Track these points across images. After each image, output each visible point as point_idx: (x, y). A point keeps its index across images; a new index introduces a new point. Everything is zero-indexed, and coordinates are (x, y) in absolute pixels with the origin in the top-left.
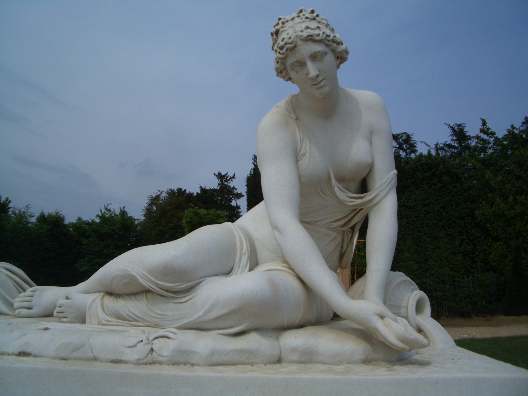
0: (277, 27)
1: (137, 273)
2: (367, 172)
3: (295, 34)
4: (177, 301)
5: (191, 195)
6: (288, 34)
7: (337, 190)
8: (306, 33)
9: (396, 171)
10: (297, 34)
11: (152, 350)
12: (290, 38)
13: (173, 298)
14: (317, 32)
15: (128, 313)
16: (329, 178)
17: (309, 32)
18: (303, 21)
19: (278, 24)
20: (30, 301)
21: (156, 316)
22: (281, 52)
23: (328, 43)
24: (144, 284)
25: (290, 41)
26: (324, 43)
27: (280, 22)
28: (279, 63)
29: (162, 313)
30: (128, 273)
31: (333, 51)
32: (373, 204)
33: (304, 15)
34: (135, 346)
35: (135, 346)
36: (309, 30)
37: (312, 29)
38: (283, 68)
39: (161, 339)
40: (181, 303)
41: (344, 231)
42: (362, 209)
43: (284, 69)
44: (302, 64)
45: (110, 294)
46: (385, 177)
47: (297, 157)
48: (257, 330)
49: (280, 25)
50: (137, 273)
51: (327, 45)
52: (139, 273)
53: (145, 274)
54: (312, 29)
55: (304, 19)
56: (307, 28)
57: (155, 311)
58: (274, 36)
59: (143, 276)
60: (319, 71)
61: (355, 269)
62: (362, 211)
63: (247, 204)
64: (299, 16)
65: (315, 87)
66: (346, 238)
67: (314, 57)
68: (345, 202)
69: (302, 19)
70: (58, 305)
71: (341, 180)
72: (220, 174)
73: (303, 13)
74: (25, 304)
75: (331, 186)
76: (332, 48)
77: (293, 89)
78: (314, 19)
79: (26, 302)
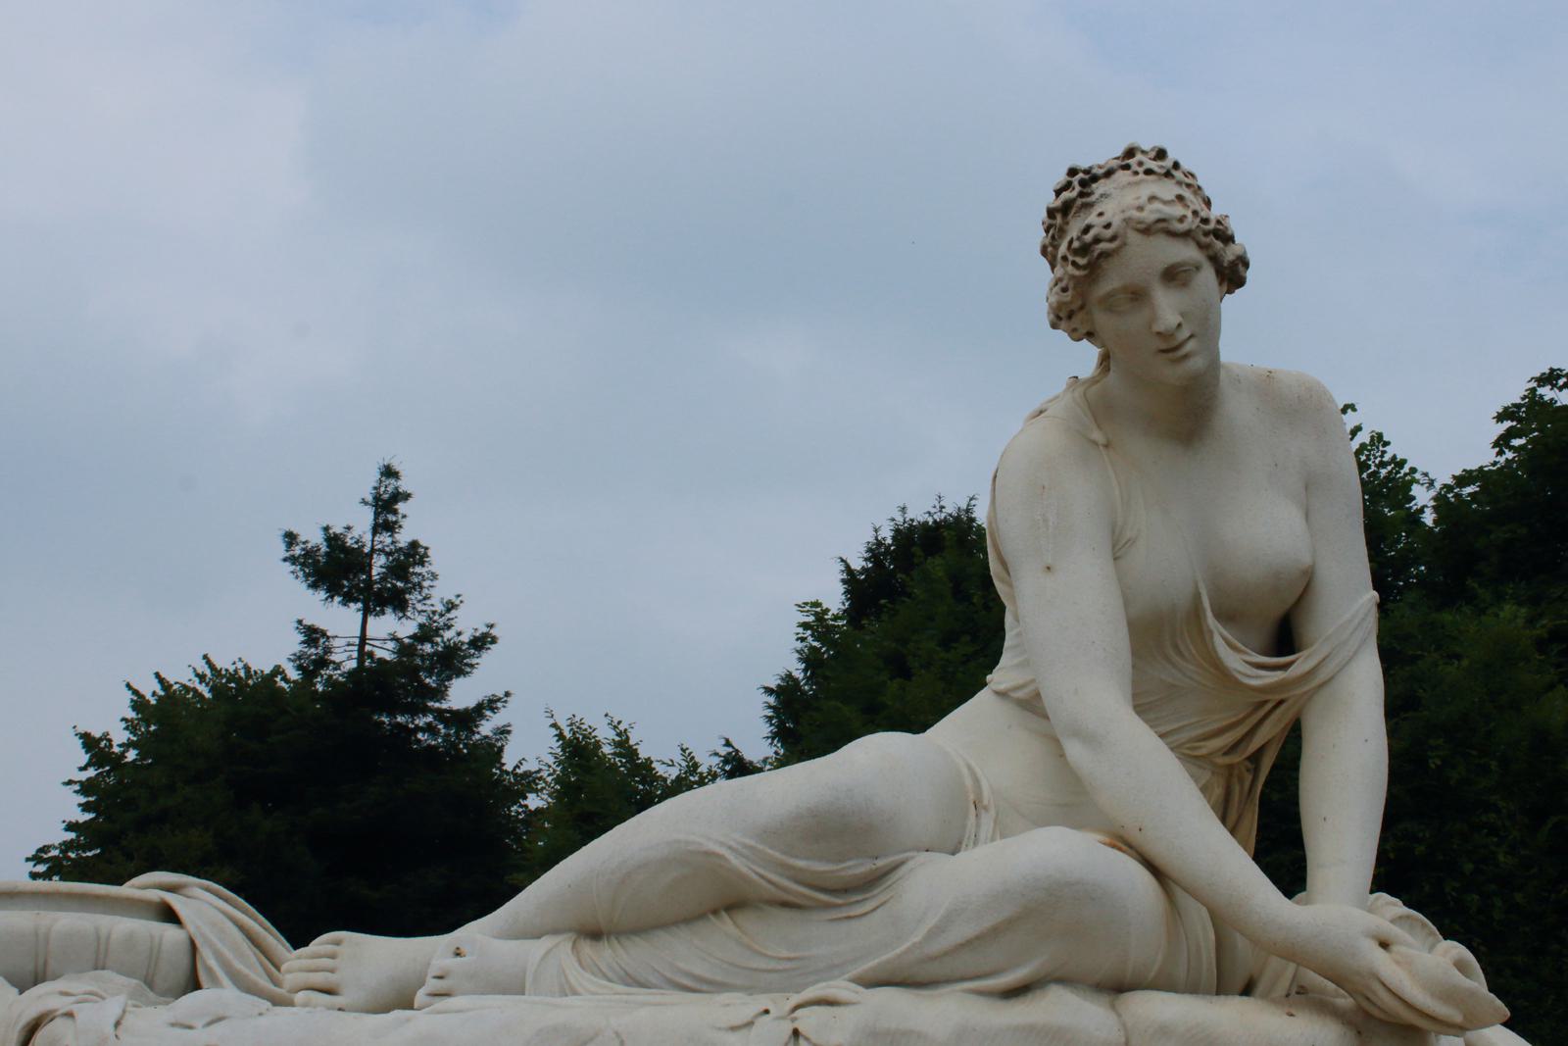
0: (1066, 195)
1: (722, 844)
2: (1291, 600)
3: (1122, 216)
4: (840, 915)
6: (1101, 214)
7: (1219, 642)
8: (1151, 212)
9: (1376, 593)
10: (1128, 214)
11: (796, 1033)
12: (1108, 226)
13: (828, 906)
14: (1178, 210)
15: (669, 975)
16: (1196, 613)
17: (1159, 211)
18: (1141, 181)
19: (1068, 186)
20: (332, 971)
21: (772, 965)
22: (1082, 261)
23: (1204, 240)
24: (744, 870)
25: (1109, 233)
26: (1194, 239)
27: (1076, 180)
28: (1070, 293)
29: (792, 955)
30: (691, 848)
31: (1215, 259)
32: (1317, 685)
33: (1140, 164)
34: (750, 1024)
35: (750, 1024)
36: (1157, 205)
37: (1165, 203)
38: (1079, 303)
39: (816, 1008)
40: (849, 918)
41: (1230, 767)
42: (1280, 703)
43: (1082, 308)
44: (1137, 295)
45: (595, 935)
46: (1349, 605)
47: (1118, 548)
48: (1063, 980)
49: (1078, 189)
50: (722, 844)
51: (1201, 246)
52: (732, 843)
53: (752, 843)
54: (1165, 203)
55: (1141, 176)
57: (769, 953)
59: (745, 851)
60: (1182, 315)
61: (1284, 858)
62: (1283, 707)
64: (1127, 167)
65: (1165, 355)
66: (1236, 789)
67: (1174, 275)
68: (1240, 677)
70: (433, 971)
71: (1226, 616)
72: (509, 732)
73: (1139, 157)
74: (319, 978)
75: (1201, 632)
76: (1211, 253)
77: (1085, 357)
78: (1168, 174)
79: (322, 971)
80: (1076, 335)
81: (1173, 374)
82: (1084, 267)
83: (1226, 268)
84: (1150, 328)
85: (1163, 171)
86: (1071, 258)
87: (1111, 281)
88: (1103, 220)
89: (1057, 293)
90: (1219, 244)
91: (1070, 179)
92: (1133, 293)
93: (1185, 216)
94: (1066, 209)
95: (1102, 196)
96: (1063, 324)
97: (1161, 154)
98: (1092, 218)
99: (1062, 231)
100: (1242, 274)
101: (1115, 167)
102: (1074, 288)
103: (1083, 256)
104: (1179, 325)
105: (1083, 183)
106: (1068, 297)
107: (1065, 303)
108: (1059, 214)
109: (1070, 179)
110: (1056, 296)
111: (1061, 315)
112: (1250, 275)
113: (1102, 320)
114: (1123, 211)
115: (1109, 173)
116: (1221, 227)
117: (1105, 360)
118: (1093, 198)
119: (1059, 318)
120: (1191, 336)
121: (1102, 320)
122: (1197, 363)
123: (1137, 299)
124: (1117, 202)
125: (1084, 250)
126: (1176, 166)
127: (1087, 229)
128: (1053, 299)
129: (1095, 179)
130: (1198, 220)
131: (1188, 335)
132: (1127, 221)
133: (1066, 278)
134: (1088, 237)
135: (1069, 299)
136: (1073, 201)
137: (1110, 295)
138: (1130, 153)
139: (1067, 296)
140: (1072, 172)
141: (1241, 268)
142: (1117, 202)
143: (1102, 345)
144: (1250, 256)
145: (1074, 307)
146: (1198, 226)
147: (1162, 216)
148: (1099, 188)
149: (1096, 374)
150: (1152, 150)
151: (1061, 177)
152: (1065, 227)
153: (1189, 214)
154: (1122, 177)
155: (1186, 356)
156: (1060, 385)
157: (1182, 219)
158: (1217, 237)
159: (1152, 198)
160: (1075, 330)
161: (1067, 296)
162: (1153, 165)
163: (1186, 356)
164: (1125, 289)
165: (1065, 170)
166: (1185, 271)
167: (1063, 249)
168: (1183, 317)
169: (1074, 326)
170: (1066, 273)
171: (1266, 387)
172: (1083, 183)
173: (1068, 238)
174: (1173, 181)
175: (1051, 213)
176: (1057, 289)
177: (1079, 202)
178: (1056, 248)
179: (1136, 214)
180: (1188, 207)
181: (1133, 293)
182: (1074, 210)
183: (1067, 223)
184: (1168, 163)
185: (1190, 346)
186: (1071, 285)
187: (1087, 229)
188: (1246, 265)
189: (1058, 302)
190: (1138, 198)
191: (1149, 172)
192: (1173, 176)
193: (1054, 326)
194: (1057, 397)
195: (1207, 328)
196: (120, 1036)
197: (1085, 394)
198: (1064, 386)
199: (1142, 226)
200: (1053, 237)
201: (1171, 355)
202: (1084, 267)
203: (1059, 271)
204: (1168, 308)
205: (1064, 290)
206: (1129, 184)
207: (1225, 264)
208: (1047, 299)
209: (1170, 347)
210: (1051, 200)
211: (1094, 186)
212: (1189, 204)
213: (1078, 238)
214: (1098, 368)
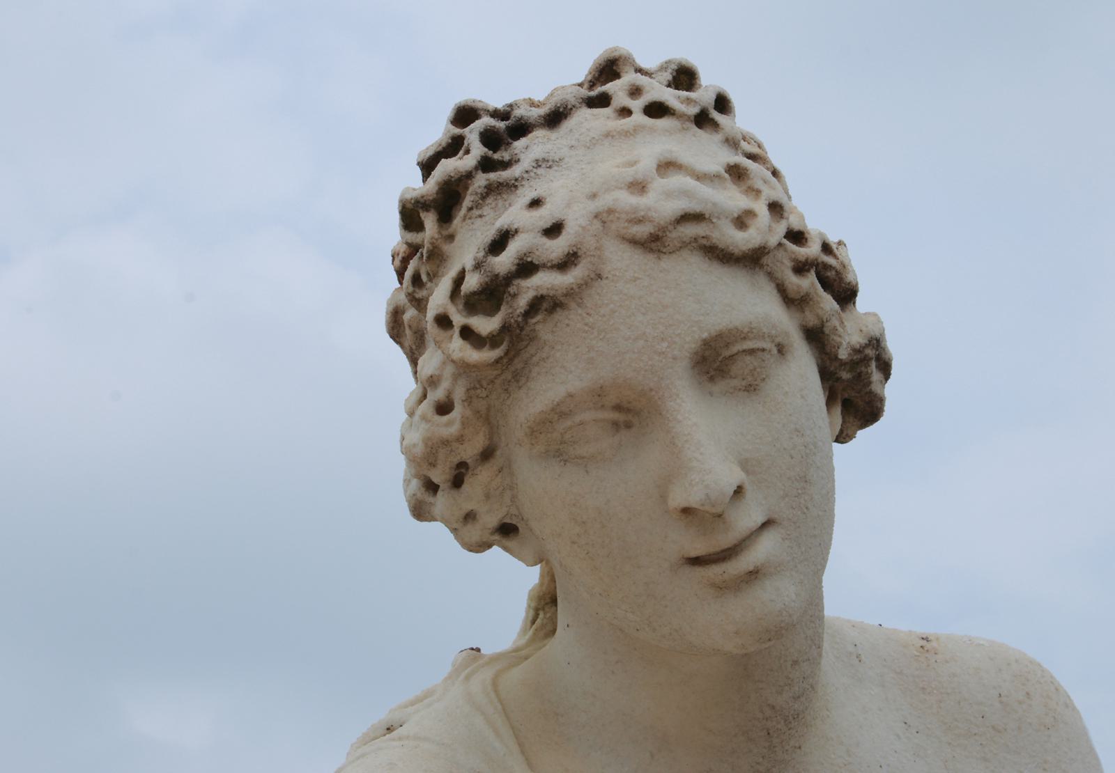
0: (447, 167)
3: (593, 206)
5: (499, 546)
6: (536, 203)
8: (669, 195)
12: (554, 230)
17: (686, 193)
18: (636, 130)
19: (454, 146)
22: (485, 325)
25: (556, 248)
26: (771, 275)
27: (472, 134)
28: (456, 414)
31: (816, 336)
33: (635, 92)
37: (700, 177)
43: (487, 455)
49: (477, 150)
51: (793, 301)
54: (700, 177)
55: (638, 118)
56: (667, 166)
58: (430, 221)
60: (745, 465)
63: (823, 589)
64: (602, 101)
67: (717, 361)
69: (625, 112)
73: (629, 77)
76: (812, 321)
78: (702, 120)
80: (475, 532)
81: (716, 621)
82: (492, 341)
83: (843, 364)
84: (663, 498)
85: (693, 110)
86: (458, 319)
87: (566, 369)
88: (544, 217)
89: (424, 418)
90: (828, 302)
91: (457, 131)
92: (618, 408)
93: (750, 213)
94: (447, 201)
95: (538, 164)
96: (441, 502)
97: (684, 77)
98: (513, 213)
99: (437, 256)
100: (875, 387)
101: (572, 101)
102: (468, 400)
103: (491, 312)
104: (739, 491)
105: (491, 139)
106: (450, 426)
107: (445, 443)
108: (435, 209)
109: (457, 131)
110: (424, 426)
111: (437, 476)
112: (893, 392)
113: (539, 484)
114: (594, 196)
115: (555, 118)
116: (830, 260)
117: (546, 603)
118: (516, 171)
119: (432, 487)
120: (767, 524)
121: (539, 484)
122: (779, 594)
123: (628, 426)
124: (573, 180)
125: (491, 295)
126: (722, 103)
127: (499, 244)
128: (415, 437)
129: (521, 129)
130: (781, 229)
131: (760, 519)
132: (603, 217)
133: (449, 370)
134: (504, 261)
135: (454, 430)
136: (469, 176)
137: (560, 412)
138: (609, 69)
139: (449, 424)
140: (465, 115)
141: (876, 376)
142: (573, 180)
143: (540, 558)
144: (893, 346)
145: (469, 452)
146: (780, 245)
147: (695, 207)
148: (529, 149)
149: (523, 641)
150: (663, 68)
151: (437, 131)
152: (446, 248)
153: (761, 208)
154: (587, 121)
155: (754, 575)
156: (435, 667)
157: (741, 221)
158: (826, 284)
159: (667, 166)
160: (470, 517)
161: (449, 424)
162: (671, 97)
163: (754, 575)
164: (598, 394)
165: (448, 112)
166: (752, 352)
167: (439, 297)
168: (747, 472)
169: (468, 506)
170: (449, 360)
171: (922, 669)
172: (491, 139)
173: (452, 273)
174: (718, 137)
175: (410, 216)
176: (427, 407)
177: (481, 180)
178: (420, 304)
179: (627, 200)
180: (758, 192)
181: (618, 408)
182: (467, 202)
183: (451, 238)
184: (704, 95)
185: (765, 549)
186: (459, 395)
187: (499, 244)
188: (885, 368)
189: (427, 441)
190: (632, 164)
191: (656, 110)
192: (715, 125)
193: (420, 512)
194: (428, 694)
195: (806, 517)
196: (904, 725)
197: (495, 683)
198: (448, 669)
199: (642, 231)
200: (417, 280)
201: (714, 571)
202: (492, 341)
203: (430, 361)
204: (709, 443)
205: (443, 408)
206: (608, 135)
207: (843, 354)
208: (403, 439)
209: (716, 555)
210: (414, 183)
211: (519, 144)
212: (759, 184)
213: (478, 266)
214: (524, 631)
